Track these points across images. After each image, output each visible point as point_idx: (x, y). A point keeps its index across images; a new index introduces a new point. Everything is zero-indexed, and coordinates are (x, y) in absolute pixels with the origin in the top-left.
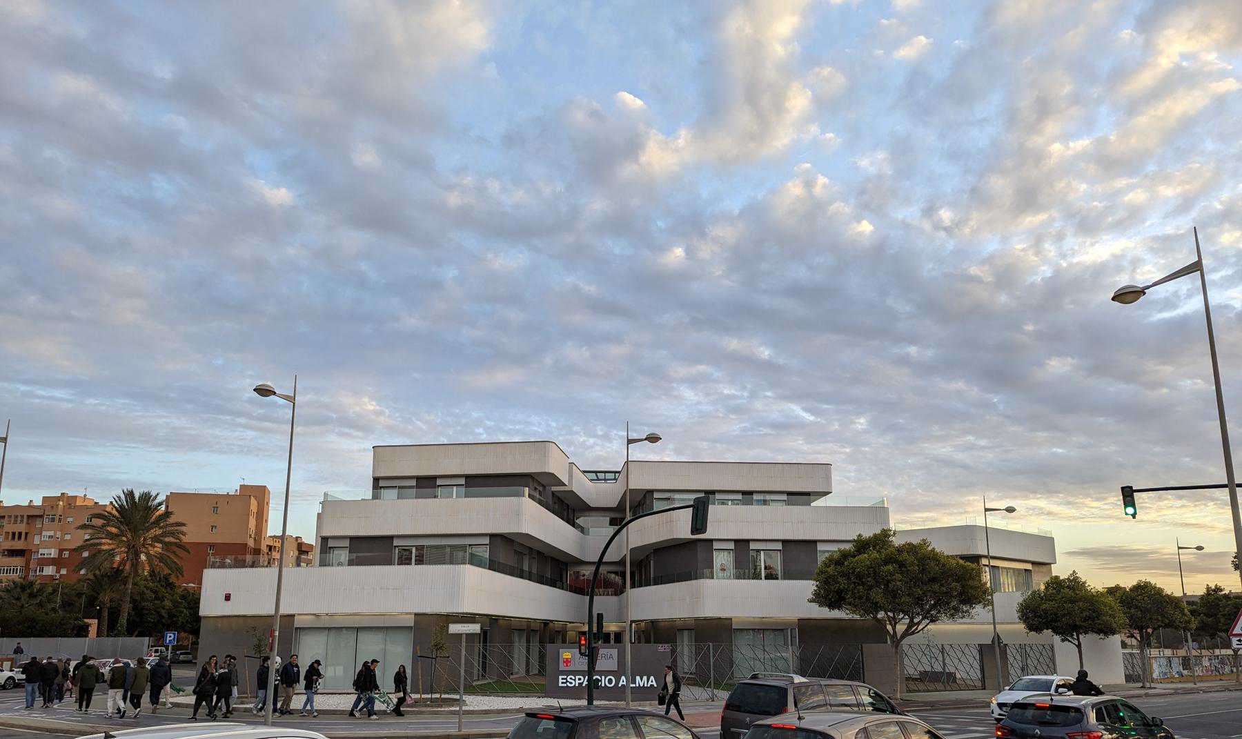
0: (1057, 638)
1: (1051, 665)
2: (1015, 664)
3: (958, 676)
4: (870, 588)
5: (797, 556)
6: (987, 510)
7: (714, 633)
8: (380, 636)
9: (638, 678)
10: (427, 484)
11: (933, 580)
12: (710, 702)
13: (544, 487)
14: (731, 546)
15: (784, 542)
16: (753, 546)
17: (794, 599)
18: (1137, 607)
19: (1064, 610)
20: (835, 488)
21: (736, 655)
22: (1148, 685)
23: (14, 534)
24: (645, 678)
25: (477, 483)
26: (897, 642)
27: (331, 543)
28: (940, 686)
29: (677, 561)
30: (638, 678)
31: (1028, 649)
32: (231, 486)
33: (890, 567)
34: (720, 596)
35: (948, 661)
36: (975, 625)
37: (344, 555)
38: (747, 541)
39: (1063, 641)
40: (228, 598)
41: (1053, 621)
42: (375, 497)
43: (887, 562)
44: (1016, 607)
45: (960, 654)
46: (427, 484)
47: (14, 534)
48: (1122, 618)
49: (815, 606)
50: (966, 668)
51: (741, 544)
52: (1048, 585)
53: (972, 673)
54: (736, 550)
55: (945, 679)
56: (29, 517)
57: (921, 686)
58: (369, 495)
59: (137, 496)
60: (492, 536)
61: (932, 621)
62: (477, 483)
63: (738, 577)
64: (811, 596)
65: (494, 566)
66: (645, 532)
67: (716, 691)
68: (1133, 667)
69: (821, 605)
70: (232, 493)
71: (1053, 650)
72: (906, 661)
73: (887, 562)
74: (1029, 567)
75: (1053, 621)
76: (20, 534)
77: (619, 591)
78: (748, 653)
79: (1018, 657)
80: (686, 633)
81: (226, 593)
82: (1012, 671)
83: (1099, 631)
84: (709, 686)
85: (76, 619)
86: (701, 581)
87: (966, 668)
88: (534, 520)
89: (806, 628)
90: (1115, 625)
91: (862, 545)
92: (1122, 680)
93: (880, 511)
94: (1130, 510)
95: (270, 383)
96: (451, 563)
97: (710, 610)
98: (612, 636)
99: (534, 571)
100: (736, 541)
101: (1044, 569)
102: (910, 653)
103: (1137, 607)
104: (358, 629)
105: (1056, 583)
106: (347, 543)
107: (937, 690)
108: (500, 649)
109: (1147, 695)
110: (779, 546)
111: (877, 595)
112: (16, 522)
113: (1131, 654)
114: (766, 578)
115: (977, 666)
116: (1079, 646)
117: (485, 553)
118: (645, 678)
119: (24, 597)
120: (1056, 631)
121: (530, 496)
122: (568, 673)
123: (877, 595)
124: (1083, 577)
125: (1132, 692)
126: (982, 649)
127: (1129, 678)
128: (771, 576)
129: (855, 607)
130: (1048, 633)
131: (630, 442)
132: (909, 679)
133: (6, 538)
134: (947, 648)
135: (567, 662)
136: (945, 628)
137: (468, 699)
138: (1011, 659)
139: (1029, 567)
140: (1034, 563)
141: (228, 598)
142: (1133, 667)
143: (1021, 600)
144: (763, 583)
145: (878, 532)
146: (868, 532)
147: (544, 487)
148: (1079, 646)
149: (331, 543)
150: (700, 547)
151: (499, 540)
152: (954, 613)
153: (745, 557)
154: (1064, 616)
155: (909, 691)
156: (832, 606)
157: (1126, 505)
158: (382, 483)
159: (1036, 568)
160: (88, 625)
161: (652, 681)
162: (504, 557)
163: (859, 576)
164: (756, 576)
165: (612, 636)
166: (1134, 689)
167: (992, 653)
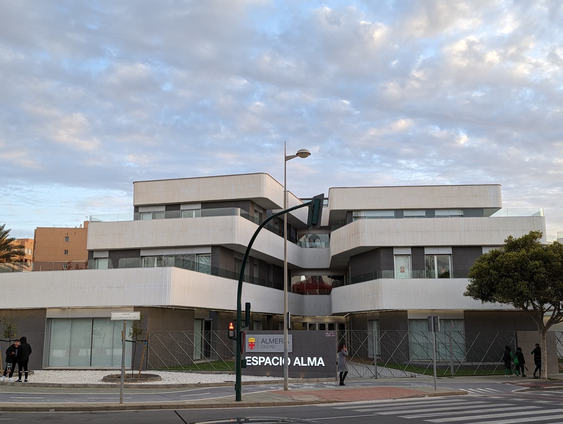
4: (518, 280)
5: (463, 256)
7: (394, 322)
8: (68, 325)
9: (309, 359)
12: (374, 380)
13: (264, 210)
14: (409, 252)
15: (454, 248)
16: (427, 251)
17: (453, 294)
20: (504, 203)
21: (412, 340)
24: (315, 359)
25: (209, 206)
26: (544, 329)
27: (95, 255)
29: (366, 263)
30: (309, 359)
32: (79, 224)
34: (396, 291)
37: (105, 263)
38: (422, 248)
46: (173, 208)
49: (470, 299)
54: (413, 256)
58: (132, 219)
60: (214, 247)
62: (209, 206)
63: (414, 276)
64: (466, 290)
65: (215, 272)
66: (343, 241)
67: (379, 369)
69: (476, 298)
70: (78, 227)
78: (421, 340)
80: (375, 324)
84: (373, 364)
86: (380, 280)
89: (470, 316)
91: (512, 245)
96: (346, 285)
97: (388, 303)
98: (327, 326)
99: (256, 275)
100: (413, 248)
104: (93, 319)
108: (217, 337)
114: (441, 276)
117: (205, 262)
118: (315, 359)
122: (252, 354)
123: (523, 286)
128: (445, 275)
131: (287, 158)
135: (252, 345)
137: (162, 374)
145: (528, 234)
147: (264, 210)
149: (95, 255)
150: (382, 253)
151: (218, 251)
153: (421, 260)
156: (485, 298)
158: (141, 210)
162: (224, 263)
165: (327, 326)
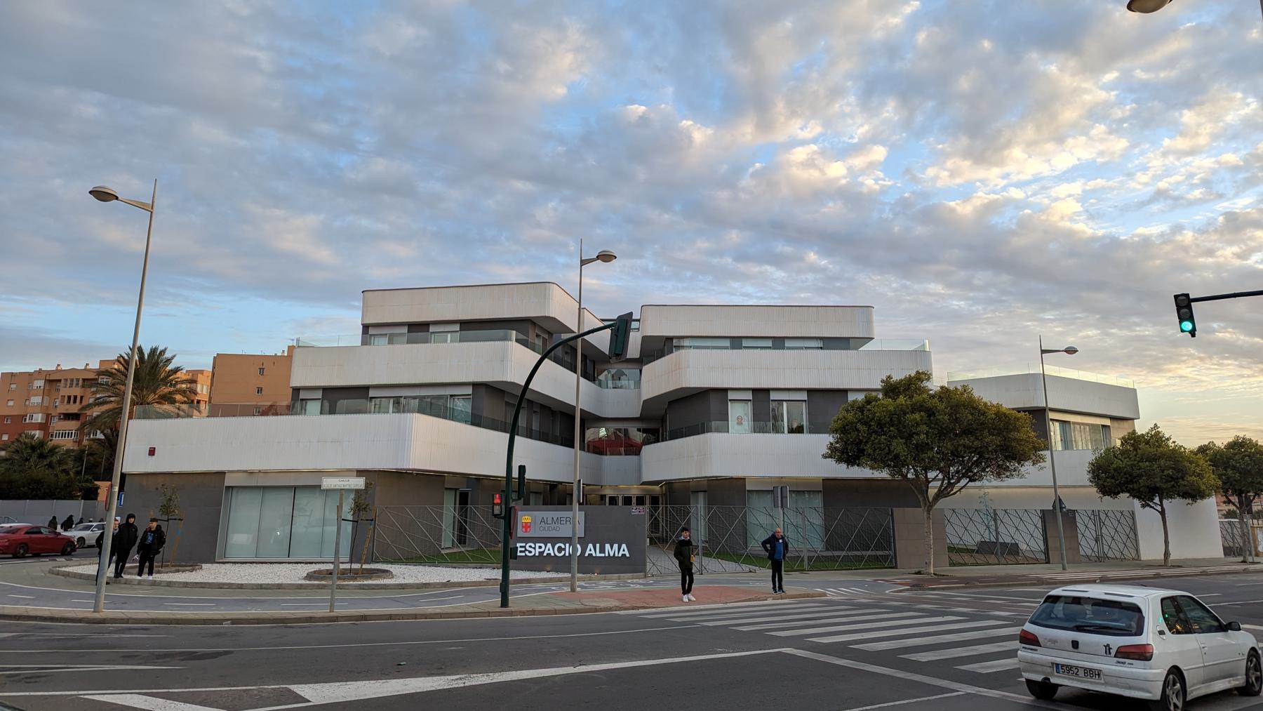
0: (1137, 503)
1: (1132, 535)
2: (1087, 534)
3: (1023, 547)
6: (1043, 352)
7: (727, 493)
8: (257, 496)
9: (608, 546)
10: (419, 329)
11: (967, 432)
13: (550, 334)
14: (749, 396)
16: (773, 396)
17: (807, 456)
18: (1234, 468)
19: (1144, 471)
20: (878, 330)
21: (751, 519)
22: (1250, 559)
23: (69, 397)
24: (616, 546)
25: (471, 327)
27: (303, 395)
28: (992, 559)
29: (688, 412)
30: (608, 546)
31: (1103, 516)
32: (277, 348)
33: (917, 416)
35: (1001, 529)
36: (1028, 483)
38: (767, 391)
39: (1143, 506)
40: (152, 452)
41: (1128, 482)
42: (364, 343)
43: (914, 409)
44: (1086, 467)
45: (1017, 521)
46: (419, 329)
47: (69, 397)
48: (1211, 478)
49: (831, 462)
50: (1030, 539)
51: (761, 394)
52: (1125, 441)
53: (1032, 543)
54: (754, 401)
55: (1011, 551)
56: (84, 380)
57: (967, 558)
59: (146, 352)
60: (475, 385)
61: (971, 481)
62: (471, 327)
63: (756, 430)
65: (476, 421)
66: (658, 379)
68: (1233, 537)
69: (839, 460)
71: (1133, 518)
72: (949, 529)
73: (914, 409)
74: (1107, 422)
75: (1128, 482)
76: (75, 397)
77: (634, 449)
78: (763, 519)
79: (1091, 525)
81: (155, 446)
82: (1083, 542)
83: (1185, 495)
85: (87, 481)
87: (1030, 539)
88: (513, 362)
89: (831, 489)
90: (1203, 487)
91: (891, 389)
92: (1220, 553)
93: (921, 354)
94: (1187, 326)
95: (111, 186)
99: (535, 426)
100: (755, 391)
101: (1126, 424)
102: (954, 519)
103: (1234, 468)
105: (1133, 440)
106: (319, 395)
107: (977, 564)
108: (481, 514)
109: (1246, 571)
110: (804, 396)
111: (899, 446)
112: (71, 386)
113: (1230, 523)
115: (1038, 534)
116: (1163, 513)
117: (462, 406)
118: (616, 546)
119: (34, 457)
120: (1136, 494)
121: (517, 341)
123: (899, 446)
124: (1166, 431)
125: (1226, 568)
126: (1044, 515)
127: (1228, 551)
129: (878, 463)
130: (1124, 496)
131: (583, 262)
132: (952, 549)
133: (62, 402)
134: (1001, 514)
136: (991, 487)
137: (394, 568)
138: (1081, 527)
139: (1107, 422)
140: (1112, 418)
141: (152, 452)
142: (1233, 537)
143: (1091, 457)
144: (785, 439)
146: (899, 375)
147: (550, 334)
148: (1163, 513)
149: (303, 395)
152: (1001, 471)
153: (764, 407)
154: (1140, 476)
155: (953, 564)
157: (1181, 319)
158: (371, 331)
159: (1116, 424)
160: (98, 488)
161: (624, 550)
162: (490, 408)
163: (880, 424)
164: (777, 430)
165: (634, 500)
166: (1234, 564)
167: (1058, 518)
